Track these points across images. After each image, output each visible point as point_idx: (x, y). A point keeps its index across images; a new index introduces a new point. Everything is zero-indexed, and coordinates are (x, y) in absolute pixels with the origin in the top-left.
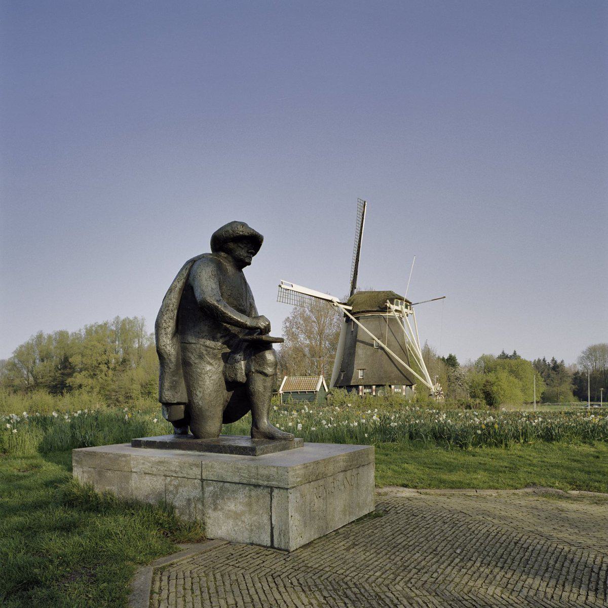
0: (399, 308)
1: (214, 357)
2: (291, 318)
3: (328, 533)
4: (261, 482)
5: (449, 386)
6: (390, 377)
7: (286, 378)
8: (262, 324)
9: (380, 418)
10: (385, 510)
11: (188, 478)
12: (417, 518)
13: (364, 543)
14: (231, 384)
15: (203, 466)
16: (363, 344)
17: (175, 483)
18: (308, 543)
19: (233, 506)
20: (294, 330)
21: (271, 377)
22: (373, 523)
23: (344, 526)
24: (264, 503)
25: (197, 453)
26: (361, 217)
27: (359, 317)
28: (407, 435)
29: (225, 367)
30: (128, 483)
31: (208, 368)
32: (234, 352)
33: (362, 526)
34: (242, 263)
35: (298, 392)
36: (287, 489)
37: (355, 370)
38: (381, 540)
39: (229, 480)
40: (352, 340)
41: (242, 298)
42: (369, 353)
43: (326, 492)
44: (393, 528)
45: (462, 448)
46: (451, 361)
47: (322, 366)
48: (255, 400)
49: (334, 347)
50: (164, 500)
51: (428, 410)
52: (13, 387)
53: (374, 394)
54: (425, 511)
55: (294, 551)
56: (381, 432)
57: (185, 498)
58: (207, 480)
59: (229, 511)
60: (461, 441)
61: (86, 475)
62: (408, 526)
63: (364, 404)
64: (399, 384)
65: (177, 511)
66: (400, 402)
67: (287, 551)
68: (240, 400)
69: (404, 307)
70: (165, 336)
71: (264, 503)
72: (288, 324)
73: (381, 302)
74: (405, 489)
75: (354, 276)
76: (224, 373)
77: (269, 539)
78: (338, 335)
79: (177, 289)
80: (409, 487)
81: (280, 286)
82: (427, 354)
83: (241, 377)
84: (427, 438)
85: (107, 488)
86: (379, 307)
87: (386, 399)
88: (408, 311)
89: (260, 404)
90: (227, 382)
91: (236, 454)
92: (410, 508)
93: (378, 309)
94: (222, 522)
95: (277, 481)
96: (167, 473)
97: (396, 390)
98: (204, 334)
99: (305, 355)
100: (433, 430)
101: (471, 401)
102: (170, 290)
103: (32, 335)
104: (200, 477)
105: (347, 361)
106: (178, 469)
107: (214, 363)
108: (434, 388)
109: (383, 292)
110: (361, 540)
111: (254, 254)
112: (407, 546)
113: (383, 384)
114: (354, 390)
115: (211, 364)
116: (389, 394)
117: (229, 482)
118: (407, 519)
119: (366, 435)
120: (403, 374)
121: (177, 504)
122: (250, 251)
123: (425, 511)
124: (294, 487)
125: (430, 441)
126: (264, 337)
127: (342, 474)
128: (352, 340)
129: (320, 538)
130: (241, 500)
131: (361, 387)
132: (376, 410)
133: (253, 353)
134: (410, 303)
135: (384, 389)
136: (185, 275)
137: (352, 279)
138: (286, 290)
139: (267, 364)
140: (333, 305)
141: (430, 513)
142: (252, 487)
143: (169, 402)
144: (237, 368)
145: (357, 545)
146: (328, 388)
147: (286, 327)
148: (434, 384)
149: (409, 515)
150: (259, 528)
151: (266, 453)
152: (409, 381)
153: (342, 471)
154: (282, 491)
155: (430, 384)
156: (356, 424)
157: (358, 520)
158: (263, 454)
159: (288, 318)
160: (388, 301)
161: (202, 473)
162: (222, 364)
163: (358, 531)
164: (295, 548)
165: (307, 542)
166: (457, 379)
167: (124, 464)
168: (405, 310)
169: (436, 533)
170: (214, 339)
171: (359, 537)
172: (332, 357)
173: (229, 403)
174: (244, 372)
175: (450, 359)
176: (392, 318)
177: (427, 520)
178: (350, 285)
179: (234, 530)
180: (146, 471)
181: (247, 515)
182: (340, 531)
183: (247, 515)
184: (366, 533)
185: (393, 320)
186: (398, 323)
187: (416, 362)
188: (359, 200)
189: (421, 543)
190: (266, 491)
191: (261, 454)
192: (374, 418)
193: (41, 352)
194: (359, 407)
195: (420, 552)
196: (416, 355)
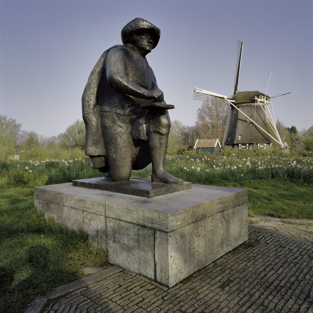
0: (262, 100)
1: (124, 121)
2: (201, 108)
3: (207, 265)
4: (146, 224)
5: (292, 144)
6: (257, 139)
7: (198, 140)
8: (156, 95)
9: (251, 163)
10: (256, 240)
11: (97, 214)
12: (285, 249)
13: (238, 280)
14: (137, 142)
15: (106, 206)
16: (241, 121)
17: (89, 217)
18: (188, 277)
19: (127, 240)
20: (203, 114)
21: (165, 136)
22: (247, 253)
23: (222, 257)
24: (149, 241)
25: (111, 193)
26: (240, 51)
27: (239, 106)
28: (270, 175)
29: (132, 129)
30: (62, 213)
31: (119, 129)
32: (139, 118)
33: (237, 256)
34: (144, 52)
35: (200, 148)
36: (167, 233)
37: (236, 135)
38: (254, 276)
39: (123, 219)
40: (235, 119)
41: (147, 78)
42: (244, 126)
43: (205, 230)
44: (265, 261)
45: (309, 184)
46: (293, 130)
47: (218, 134)
48: (154, 153)
49: (225, 123)
50: (82, 228)
51: (282, 158)
52: (66, 146)
53: (248, 148)
54: (291, 242)
55: (173, 287)
56: (252, 172)
57: (95, 229)
58: (109, 217)
59: (124, 244)
60: (309, 180)
61: (40, 205)
62: (277, 260)
63: (241, 155)
64: (262, 143)
65: (90, 238)
66: (263, 153)
67: (167, 286)
68: (144, 155)
69: (265, 99)
70: (88, 107)
71: (149, 241)
72: (200, 112)
73: (252, 97)
74: (272, 218)
75: (236, 84)
76: (131, 133)
77: (153, 273)
78: (227, 116)
79: (97, 72)
80: (275, 216)
81: (195, 91)
82: (279, 126)
83: (143, 137)
84: (284, 177)
85: (51, 215)
86: (250, 100)
87: (255, 151)
88: (268, 102)
89: (157, 157)
90: (134, 140)
91: (136, 195)
92: (278, 239)
93: (250, 101)
94: (119, 252)
95: (159, 225)
96: (84, 209)
97: (260, 146)
98: (116, 105)
99: (209, 128)
100: (288, 170)
101: (306, 152)
102: (92, 73)
103: (74, 121)
104: (104, 215)
105: (232, 130)
106: (90, 207)
107: (123, 126)
108: (283, 145)
109: (253, 92)
110: (236, 275)
111: (154, 48)
112: (279, 288)
113: (253, 143)
114: (236, 147)
115: (121, 127)
116: (256, 149)
117: (123, 221)
118: (276, 251)
119: (242, 175)
120: (264, 137)
121: (90, 233)
122: (150, 41)
123: (291, 242)
124: (174, 230)
125: (286, 179)
126: (157, 104)
127: (220, 214)
128: (235, 119)
129: (199, 271)
130: (132, 237)
131: (240, 145)
132: (249, 158)
133: (151, 117)
134: (269, 97)
135: (253, 146)
136: (102, 61)
137: (235, 85)
138: (198, 93)
139: (162, 125)
140: (224, 100)
141: (295, 245)
142: (140, 227)
143: (92, 155)
144: (140, 129)
145: (232, 281)
146: (221, 145)
147: (199, 113)
148: (283, 143)
149: (277, 247)
150: (145, 262)
151: (158, 195)
152: (268, 141)
153: (220, 212)
154: (163, 233)
155: (281, 143)
156: (235, 167)
157: (234, 250)
158: (156, 196)
159: (200, 108)
160: (256, 96)
161: (105, 211)
162: (130, 127)
163: (233, 263)
164: (175, 283)
165: (187, 276)
166: (297, 140)
167: (60, 199)
168: (266, 101)
169: (305, 271)
170: (123, 108)
171: (234, 272)
172: (224, 128)
173: (138, 156)
174: (145, 132)
175: (292, 128)
176: (257, 106)
177: (294, 252)
178: (234, 88)
179: (128, 261)
180: (72, 206)
181: (136, 249)
182: (218, 262)
183: (136, 249)
184: (240, 266)
185: (258, 107)
186: (261, 108)
187: (272, 130)
188: (239, 41)
189: (292, 284)
190: (150, 232)
191: (154, 196)
192: (248, 163)
193: (78, 129)
194: (239, 156)
195: (293, 297)
196: (272, 126)
